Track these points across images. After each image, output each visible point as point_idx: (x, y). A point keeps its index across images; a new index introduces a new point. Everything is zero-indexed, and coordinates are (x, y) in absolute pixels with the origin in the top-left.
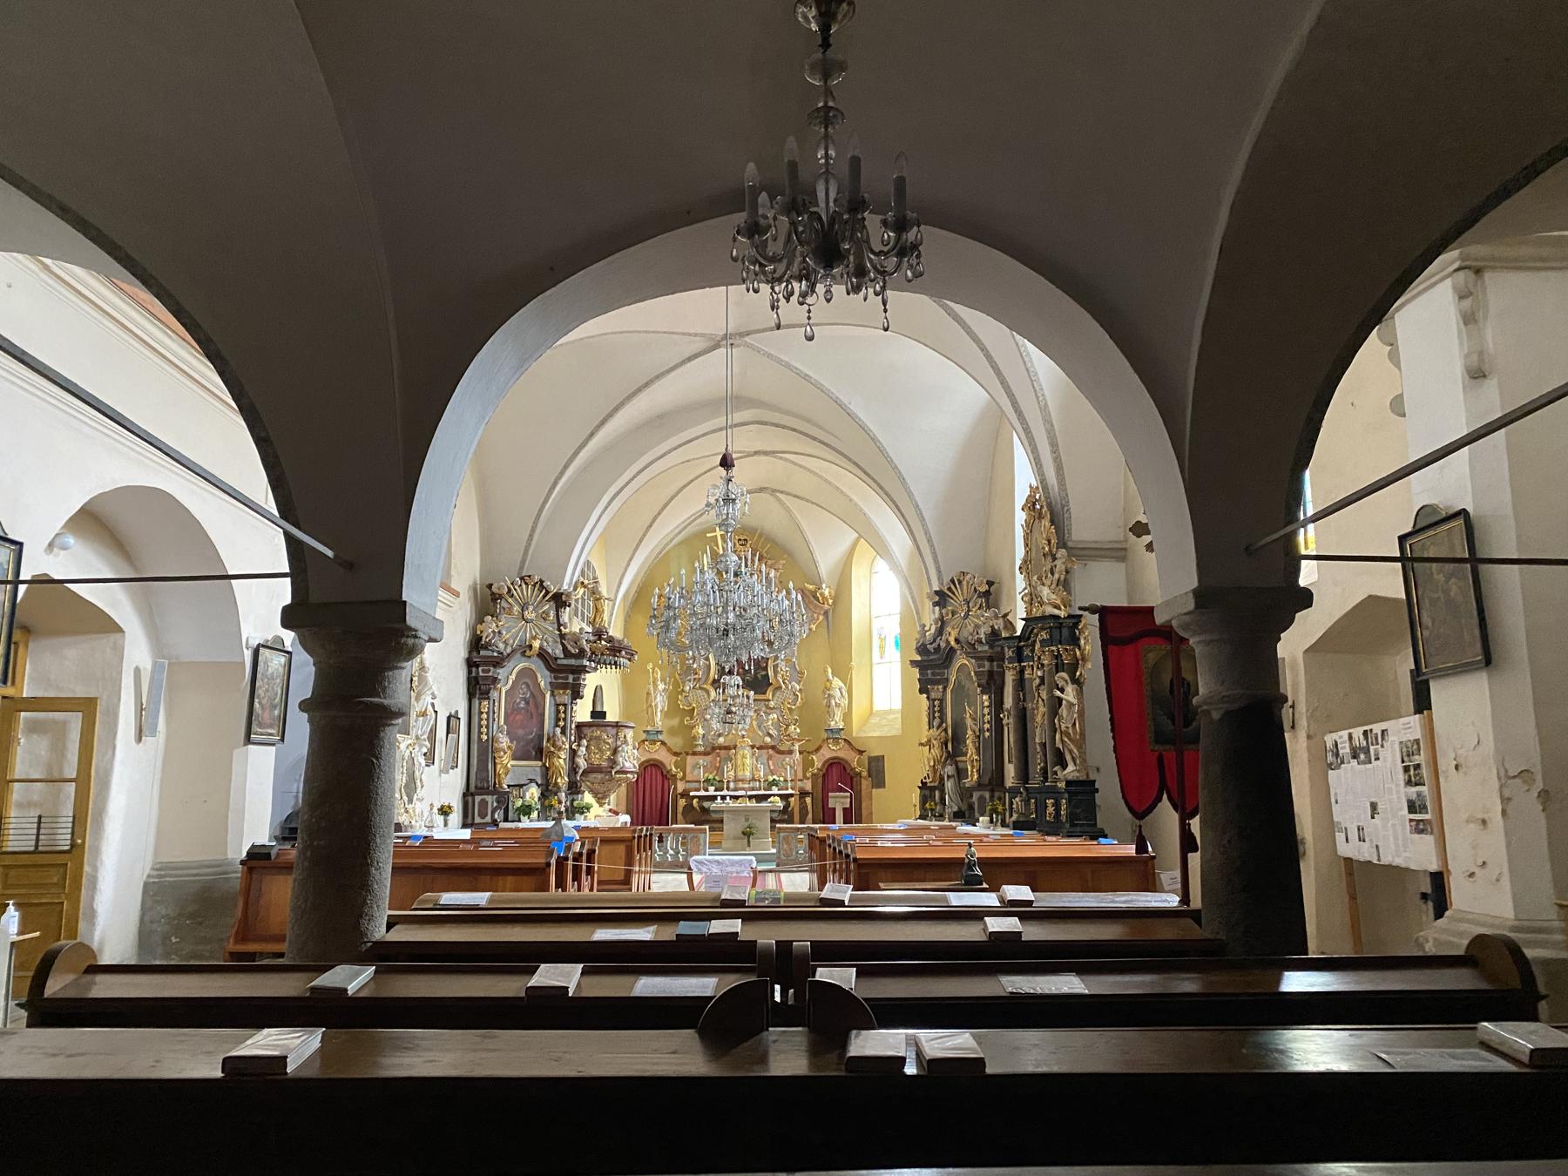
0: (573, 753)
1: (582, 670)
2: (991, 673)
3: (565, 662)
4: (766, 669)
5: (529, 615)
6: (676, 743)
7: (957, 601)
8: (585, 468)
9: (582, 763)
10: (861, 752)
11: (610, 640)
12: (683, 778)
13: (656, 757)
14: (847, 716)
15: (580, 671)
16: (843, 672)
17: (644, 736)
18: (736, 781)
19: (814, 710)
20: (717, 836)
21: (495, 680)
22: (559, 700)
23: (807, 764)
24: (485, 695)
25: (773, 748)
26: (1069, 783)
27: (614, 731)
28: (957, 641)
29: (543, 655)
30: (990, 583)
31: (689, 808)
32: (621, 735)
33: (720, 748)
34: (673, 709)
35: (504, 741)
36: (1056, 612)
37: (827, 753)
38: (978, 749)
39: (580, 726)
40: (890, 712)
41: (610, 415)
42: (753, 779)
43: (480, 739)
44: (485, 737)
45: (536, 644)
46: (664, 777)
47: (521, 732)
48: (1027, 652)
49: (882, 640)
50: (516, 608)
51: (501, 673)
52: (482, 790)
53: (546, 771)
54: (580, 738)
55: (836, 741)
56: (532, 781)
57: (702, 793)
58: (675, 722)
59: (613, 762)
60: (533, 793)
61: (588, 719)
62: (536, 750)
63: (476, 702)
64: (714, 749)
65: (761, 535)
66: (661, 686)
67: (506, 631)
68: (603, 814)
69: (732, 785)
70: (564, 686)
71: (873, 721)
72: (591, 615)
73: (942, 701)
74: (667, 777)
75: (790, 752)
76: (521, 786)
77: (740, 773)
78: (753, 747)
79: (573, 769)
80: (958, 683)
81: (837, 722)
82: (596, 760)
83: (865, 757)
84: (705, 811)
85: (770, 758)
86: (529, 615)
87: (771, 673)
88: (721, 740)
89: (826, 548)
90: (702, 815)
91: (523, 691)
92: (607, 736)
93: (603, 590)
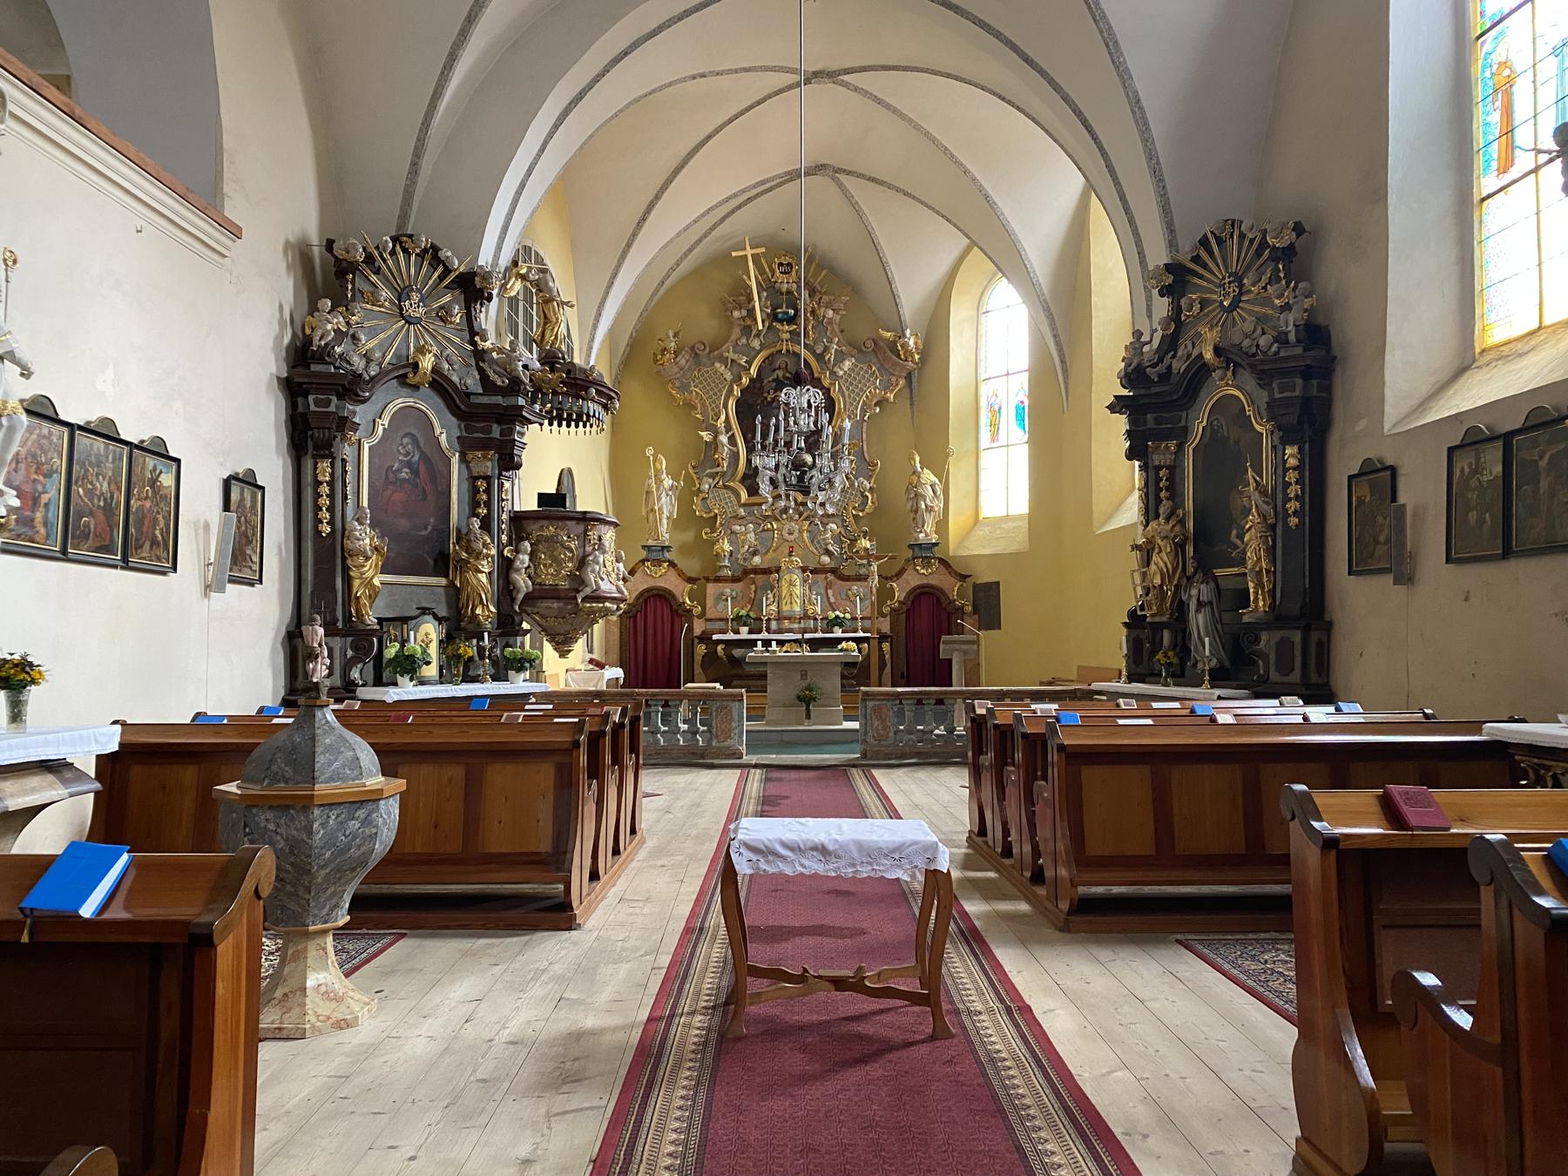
0: (506, 566)
2: (1306, 401)
3: (485, 400)
5: (414, 308)
6: (692, 566)
7: (1212, 285)
9: (522, 582)
10: (963, 577)
11: (571, 368)
12: (702, 615)
13: (661, 584)
14: (942, 526)
15: (513, 418)
16: (939, 464)
17: (643, 554)
18: (779, 619)
19: (892, 520)
20: (758, 699)
21: (344, 424)
23: (884, 593)
24: (325, 450)
25: (834, 571)
27: (580, 528)
28: (1218, 351)
29: (440, 384)
30: (1299, 229)
31: (711, 657)
32: (593, 535)
33: (757, 571)
35: (364, 537)
37: (912, 580)
38: (1271, 552)
39: (518, 519)
40: (1007, 518)
42: (806, 616)
43: (318, 533)
45: (427, 363)
47: (404, 524)
49: (996, 413)
51: (361, 414)
55: (927, 562)
56: (424, 611)
57: (731, 636)
58: (689, 536)
59: (578, 581)
60: (429, 633)
61: (533, 505)
62: (437, 555)
64: (746, 572)
67: (371, 335)
68: (570, 668)
69: (774, 625)
70: (485, 445)
71: (980, 532)
72: (536, 331)
73: (1174, 469)
74: (678, 613)
75: (862, 578)
76: (404, 620)
77: (785, 608)
78: (804, 570)
79: (506, 590)
80: (1213, 437)
81: (928, 533)
82: (548, 576)
84: (737, 662)
85: (828, 586)
86: (414, 308)
88: (757, 560)
89: (914, 264)
90: (733, 668)
92: (569, 539)
93: (562, 285)
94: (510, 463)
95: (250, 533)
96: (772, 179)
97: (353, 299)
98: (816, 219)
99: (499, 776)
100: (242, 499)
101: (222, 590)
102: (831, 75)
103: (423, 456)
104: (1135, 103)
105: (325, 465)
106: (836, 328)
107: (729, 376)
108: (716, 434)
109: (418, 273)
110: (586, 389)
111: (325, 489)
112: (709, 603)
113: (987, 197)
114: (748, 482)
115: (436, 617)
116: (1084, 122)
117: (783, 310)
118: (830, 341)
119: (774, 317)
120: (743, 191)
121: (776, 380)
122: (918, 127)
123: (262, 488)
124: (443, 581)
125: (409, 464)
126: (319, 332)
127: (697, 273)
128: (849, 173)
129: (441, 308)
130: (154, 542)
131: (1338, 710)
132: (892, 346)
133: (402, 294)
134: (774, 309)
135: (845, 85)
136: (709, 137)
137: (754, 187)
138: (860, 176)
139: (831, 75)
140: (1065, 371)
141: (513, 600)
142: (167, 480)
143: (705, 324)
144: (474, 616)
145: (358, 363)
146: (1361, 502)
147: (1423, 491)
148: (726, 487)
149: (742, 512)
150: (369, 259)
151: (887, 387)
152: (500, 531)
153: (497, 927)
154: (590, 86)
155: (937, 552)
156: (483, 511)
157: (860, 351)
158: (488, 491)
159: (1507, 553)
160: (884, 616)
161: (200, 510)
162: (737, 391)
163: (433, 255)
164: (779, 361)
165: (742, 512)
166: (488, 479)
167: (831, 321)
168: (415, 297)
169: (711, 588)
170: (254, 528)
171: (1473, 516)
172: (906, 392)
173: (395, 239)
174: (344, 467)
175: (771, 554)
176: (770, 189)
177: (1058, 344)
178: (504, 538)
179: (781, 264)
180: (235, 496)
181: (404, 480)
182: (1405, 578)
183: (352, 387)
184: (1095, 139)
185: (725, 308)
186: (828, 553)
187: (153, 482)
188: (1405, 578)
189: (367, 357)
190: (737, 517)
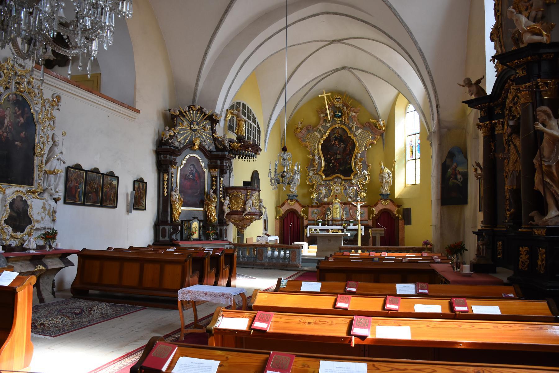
0: (221, 204)
3: (215, 153)
6: (306, 201)
9: (227, 210)
12: (307, 219)
22: (213, 174)
24: (167, 171)
26: (551, 230)
29: (202, 148)
34: (303, 184)
36: (536, 38)
44: (166, 194)
46: (298, 218)
48: (498, 111)
51: (178, 159)
52: (165, 223)
53: (205, 212)
55: (386, 200)
56: (195, 218)
59: (244, 210)
63: (162, 174)
65: (347, 96)
67: (181, 134)
69: (330, 222)
70: (215, 167)
76: (188, 221)
79: (221, 212)
81: (386, 190)
87: (353, 165)
95: (142, 196)
96: (328, 72)
97: (176, 126)
98: (348, 83)
99: (169, 269)
100: (139, 186)
101: (131, 212)
102: (339, 41)
103: (197, 171)
104: (420, 51)
105: (166, 176)
106: (356, 119)
107: (319, 136)
108: (314, 156)
109: (196, 116)
111: (166, 182)
112: (309, 214)
113: (398, 75)
114: (325, 172)
115: (198, 220)
117: (338, 113)
118: (353, 123)
119: (334, 116)
120: (318, 77)
121: (335, 137)
122: (371, 55)
123: (146, 183)
124: (202, 209)
125: (192, 174)
126: (164, 137)
128: (354, 69)
129: (203, 126)
130: (110, 200)
133: (191, 123)
136: (302, 62)
137: (322, 75)
139: (339, 41)
141: (223, 215)
142: (115, 183)
143: (313, 119)
144: (211, 220)
145: (177, 144)
149: (323, 183)
150: (181, 113)
151: (373, 138)
152: (220, 194)
153: (161, 308)
154: (251, 55)
155: (390, 197)
156: (214, 187)
157: (364, 126)
158: (216, 181)
160: (370, 220)
161: (125, 189)
162: (322, 141)
163: (201, 110)
164: (336, 131)
165: (323, 183)
166: (216, 177)
167: (354, 117)
168: (195, 124)
169: (310, 210)
170: (143, 194)
172: (381, 140)
173: (189, 107)
174: (172, 177)
176: (329, 75)
177: (427, 124)
178: (221, 196)
179: (336, 98)
180: (136, 186)
181: (190, 179)
183: (177, 152)
187: (110, 184)
189: (180, 142)
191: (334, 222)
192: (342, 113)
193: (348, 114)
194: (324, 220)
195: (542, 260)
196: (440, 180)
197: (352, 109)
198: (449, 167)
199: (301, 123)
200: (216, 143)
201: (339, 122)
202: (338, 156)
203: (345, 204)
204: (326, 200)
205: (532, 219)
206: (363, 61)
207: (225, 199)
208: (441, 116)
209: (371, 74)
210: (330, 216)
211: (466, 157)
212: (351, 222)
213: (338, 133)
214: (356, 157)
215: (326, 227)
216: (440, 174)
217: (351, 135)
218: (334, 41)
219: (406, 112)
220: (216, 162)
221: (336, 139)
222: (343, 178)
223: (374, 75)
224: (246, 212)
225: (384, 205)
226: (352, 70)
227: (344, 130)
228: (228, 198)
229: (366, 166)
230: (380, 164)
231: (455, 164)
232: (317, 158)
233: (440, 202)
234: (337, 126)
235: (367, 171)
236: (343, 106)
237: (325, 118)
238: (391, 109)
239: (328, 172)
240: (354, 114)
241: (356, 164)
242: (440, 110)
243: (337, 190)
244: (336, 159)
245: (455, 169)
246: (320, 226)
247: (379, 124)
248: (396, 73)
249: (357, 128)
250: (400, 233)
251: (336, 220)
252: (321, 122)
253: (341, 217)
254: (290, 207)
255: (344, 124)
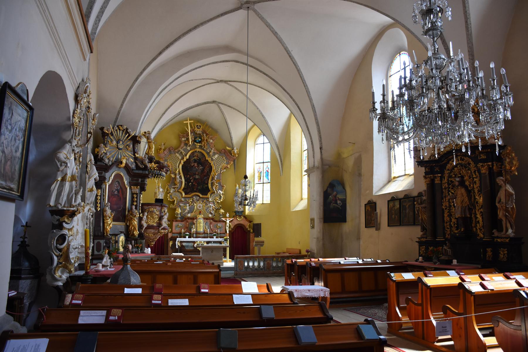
0: (140, 219)
1: (147, 176)
3: (137, 172)
4: (207, 184)
8: (150, 74)
9: (145, 225)
10: (250, 222)
12: (171, 232)
24: (101, 188)
25: (212, 219)
29: (127, 167)
33: (189, 218)
35: (108, 211)
41: (171, 44)
42: (204, 233)
50: (115, 143)
53: (127, 227)
54: (143, 212)
55: (240, 216)
56: (121, 232)
64: (186, 219)
65: (207, 125)
66: (161, 190)
67: (108, 152)
69: (195, 235)
70: (136, 185)
76: (116, 235)
79: (140, 226)
83: (252, 224)
91: (116, 186)
94: (143, 189)
98: (212, 115)
102: (226, 82)
104: (313, 106)
107: (180, 158)
108: (175, 175)
110: (163, 169)
112: (174, 228)
113: (263, 115)
116: (298, 107)
117: (198, 138)
119: (195, 141)
121: (195, 160)
125: (117, 190)
127: (172, 125)
131: (345, 259)
132: (230, 152)
134: (195, 139)
135: (228, 84)
136: (187, 93)
138: (225, 105)
139: (226, 82)
140: (282, 164)
141: (142, 229)
143: (174, 142)
144: (133, 234)
146: (368, 210)
147: (382, 210)
148: (178, 192)
149: (183, 199)
151: (228, 163)
156: (135, 203)
157: (220, 152)
158: (137, 198)
159: (400, 225)
162: (182, 162)
163: (126, 131)
164: (195, 154)
165: (183, 199)
166: (137, 194)
168: (121, 143)
171: (393, 216)
172: (233, 165)
175: (193, 213)
182: (378, 229)
184: (301, 111)
185: (180, 137)
186: (211, 214)
188: (378, 229)
190: (181, 201)
191: (198, 235)
192: (201, 139)
193: (207, 140)
194: (190, 233)
195: (504, 254)
196: (322, 204)
197: (210, 137)
198: (330, 194)
199: (164, 144)
200: (137, 162)
201: (198, 147)
202: (197, 177)
203: (207, 219)
204: (189, 215)
205: (493, 234)
206: (236, 99)
207: (143, 215)
208: (323, 156)
209: (236, 110)
210: (195, 230)
211: (344, 188)
212: (215, 235)
213: (198, 156)
214: (213, 179)
215: (192, 239)
216: (322, 199)
217: (209, 159)
218: (221, 81)
219: (255, 144)
220: (138, 180)
221: (195, 161)
222: (201, 196)
223: (238, 111)
224: (162, 227)
225: (240, 220)
226: (220, 105)
227: (203, 154)
228: (146, 214)
229: (221, 187)
230: (236, 186)
231: (335, 193)
232: (178, 177)
233: (322, 220)
234: (198, 150)
235: (222, 191)
236: (203, 133)
237: (187, 142)
238: (244, 139)
239: (187, 190)
240: (211, 141)
241: (212, 184)
242: (323, 151)
243: (200, 207)
244: (195, 179)
245: (335, 196)
246: (187, 239)
247: (234, 152)
248: (261, 113)
249: (214, 154)
250: (251, 244)
251: (199, 233)
252: (182, 145)
253: (204, 231)
254: (239, 223)
255: (203, 149)
